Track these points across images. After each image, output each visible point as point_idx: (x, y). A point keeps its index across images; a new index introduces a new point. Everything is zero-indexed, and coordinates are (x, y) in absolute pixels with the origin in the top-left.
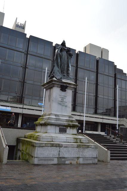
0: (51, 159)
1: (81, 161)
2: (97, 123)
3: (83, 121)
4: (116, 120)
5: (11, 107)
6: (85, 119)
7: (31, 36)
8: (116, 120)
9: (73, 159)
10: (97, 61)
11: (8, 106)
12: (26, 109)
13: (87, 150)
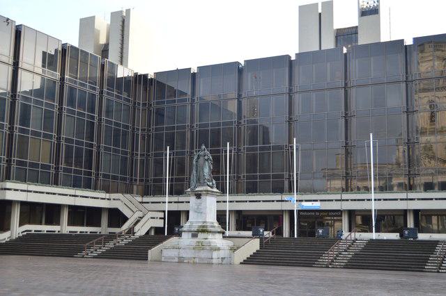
0: (173, 258)
1: (197, 260)
2: (98, 211)
3: (370, 211)
4: (163, 202)
5: (321, 201)
6: (373, 206)
7: (415, 39)
8: (163, 202)
9: (190, 258)
10: (18, 33)
11: (316, 201)
12: (347, 200)
13: (202, 251)
